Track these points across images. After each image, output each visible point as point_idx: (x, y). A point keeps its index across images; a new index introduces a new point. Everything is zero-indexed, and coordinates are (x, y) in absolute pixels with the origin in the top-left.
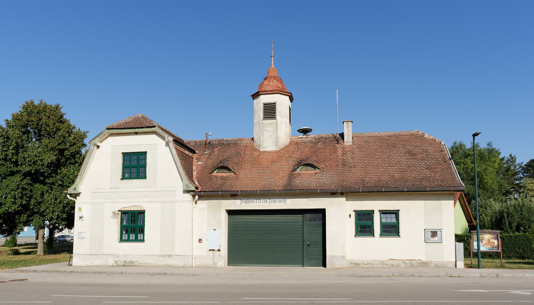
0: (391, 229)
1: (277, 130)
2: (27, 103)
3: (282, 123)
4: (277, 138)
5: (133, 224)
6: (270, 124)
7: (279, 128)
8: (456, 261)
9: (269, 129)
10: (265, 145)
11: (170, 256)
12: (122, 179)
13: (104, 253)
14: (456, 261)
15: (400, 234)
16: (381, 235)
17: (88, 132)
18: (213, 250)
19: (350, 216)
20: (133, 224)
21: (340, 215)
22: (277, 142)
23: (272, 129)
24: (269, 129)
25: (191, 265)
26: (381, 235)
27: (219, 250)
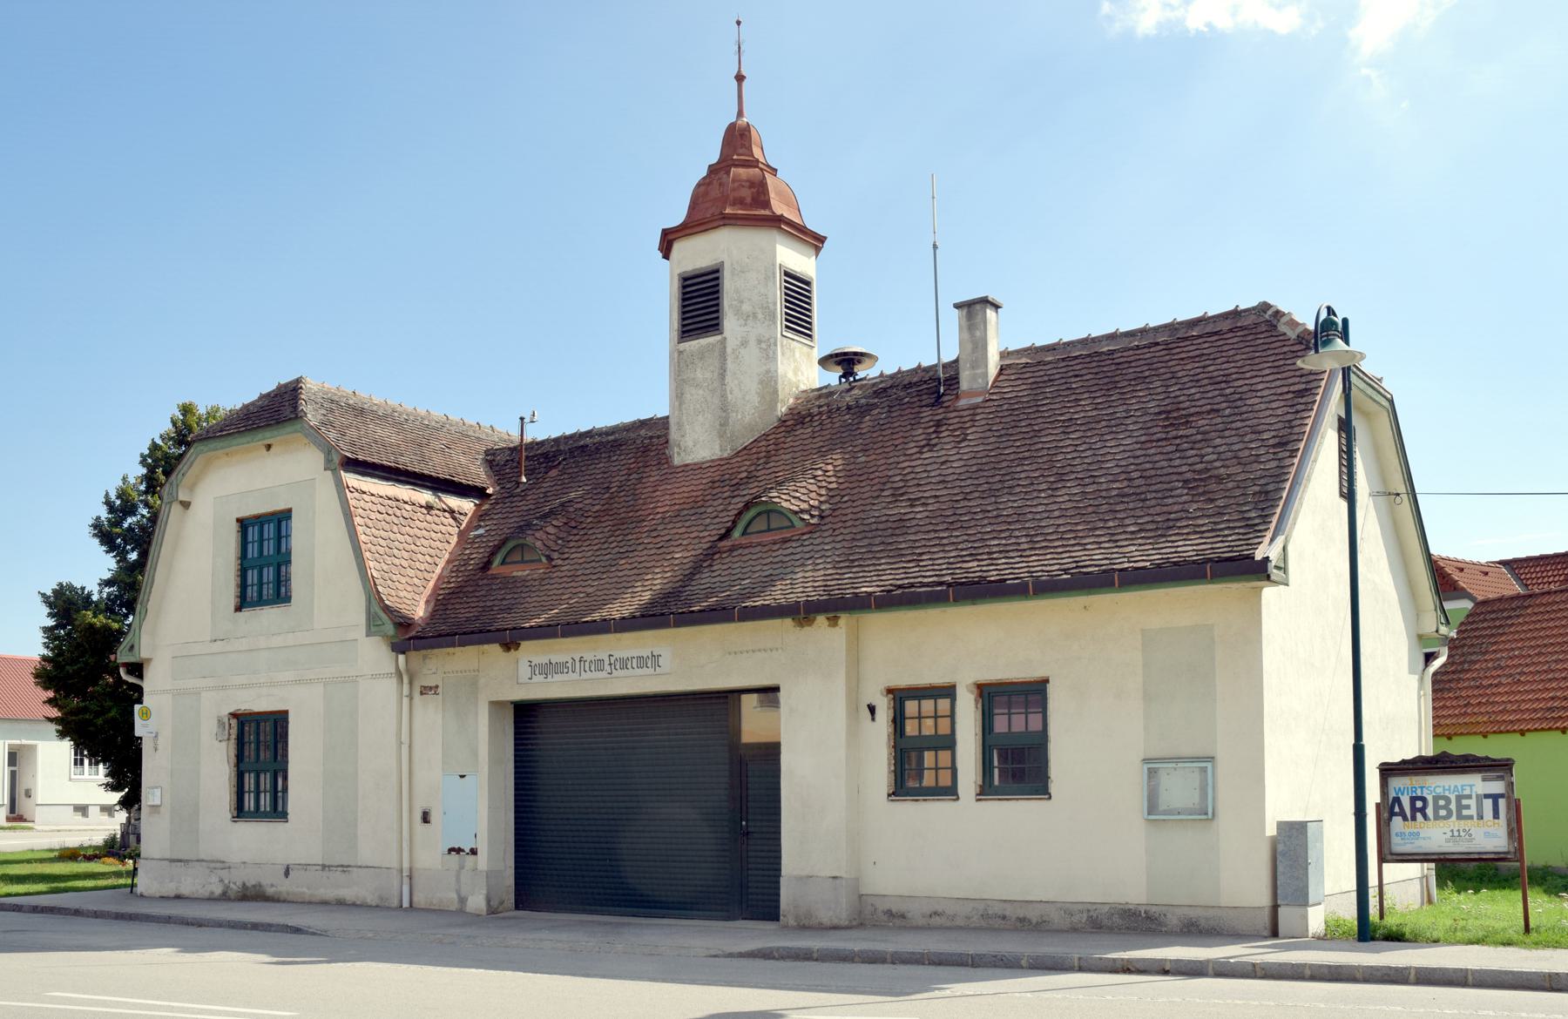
0: (1019, 766)
1: (723, 375)
2: (60, 585)
3: (744, 343)
4: (724, 408)
5: (260, 745)
6: (702, 355)
7: (730, 365)
8: (1275, 908)
9: (699, 375)
10: (688, 441)
11: (345, 868)
12: (238, 609)
13: (202, 856)
14: (1275, 908)
15: (1053, 788)
16: (986, 790)
17: (43, 595)
18: (459, 851)
19: (872, 709)
20: (260, 745)
21: (819, 707)
22: (724, 424)
23: (708, 375)
24: (699, 375)
25: (395, 903)
26: (986, 790)
27: (474, 852)
